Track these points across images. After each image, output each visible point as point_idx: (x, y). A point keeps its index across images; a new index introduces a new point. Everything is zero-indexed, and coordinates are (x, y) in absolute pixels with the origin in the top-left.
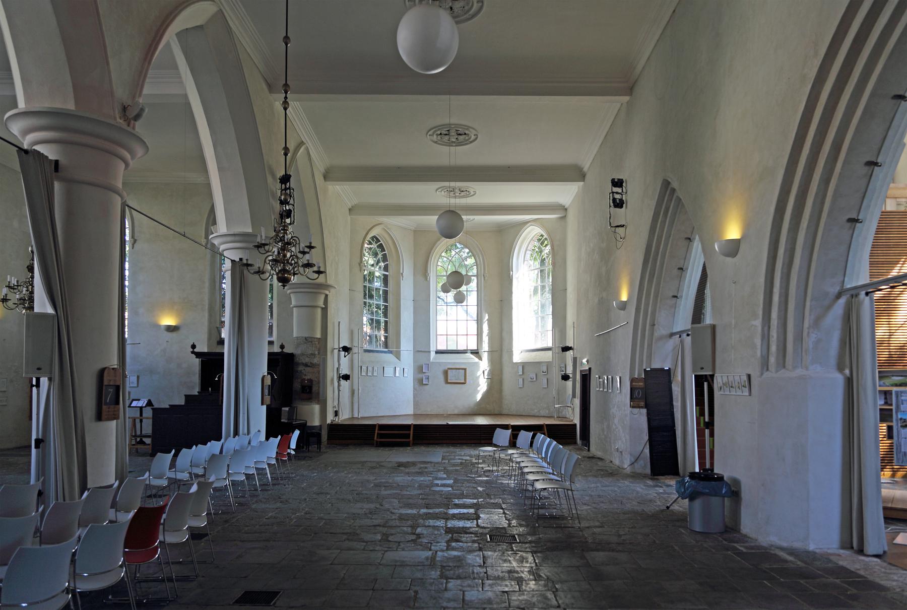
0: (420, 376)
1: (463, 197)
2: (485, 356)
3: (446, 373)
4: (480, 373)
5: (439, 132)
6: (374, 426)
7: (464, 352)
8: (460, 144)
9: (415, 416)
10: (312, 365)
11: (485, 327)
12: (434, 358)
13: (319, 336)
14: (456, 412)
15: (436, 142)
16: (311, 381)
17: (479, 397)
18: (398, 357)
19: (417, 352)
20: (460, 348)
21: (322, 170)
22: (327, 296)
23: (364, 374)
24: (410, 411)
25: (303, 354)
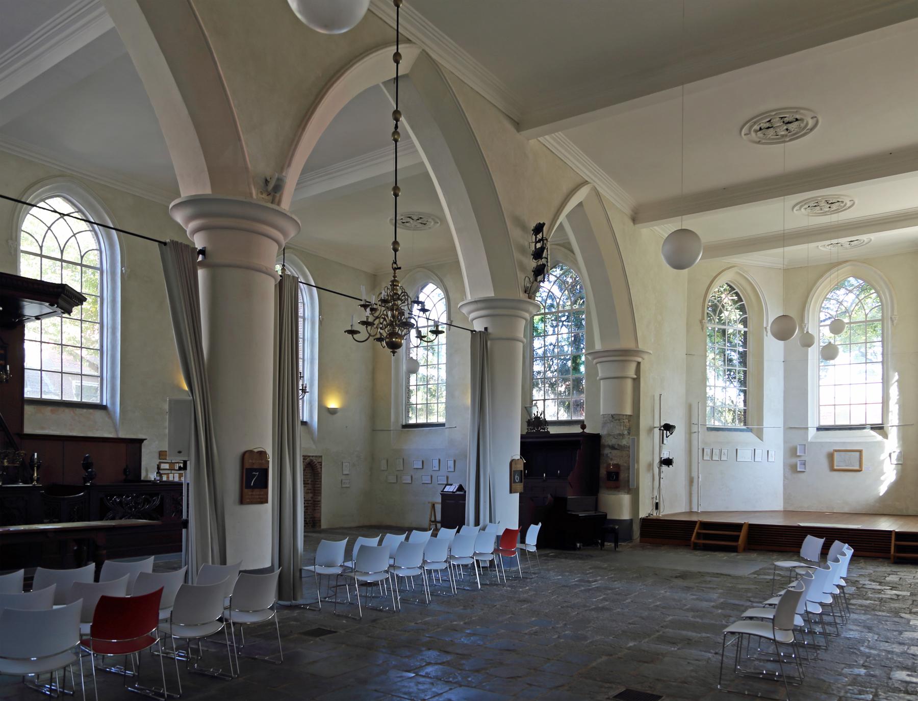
0: (794, 460)
1: (837, 211)
2: (893, 433)
3: (831, 456)
4: (884, 456)
5: (757, 127)
6: (695, 522)
7: (861, 427)
8: (795, 137)
9: (787, 513)
10: (620, 448)
11: (894, 392)
13: (628, 411)
14: (846, 510)
15: (759, 142)
16: (617, 466)
17: (883, 489)
20: (854, 422)
21: (628, 211)
22: (639, 363)
23: (707, 458)
24: (779, 505)
25: (609, 435)
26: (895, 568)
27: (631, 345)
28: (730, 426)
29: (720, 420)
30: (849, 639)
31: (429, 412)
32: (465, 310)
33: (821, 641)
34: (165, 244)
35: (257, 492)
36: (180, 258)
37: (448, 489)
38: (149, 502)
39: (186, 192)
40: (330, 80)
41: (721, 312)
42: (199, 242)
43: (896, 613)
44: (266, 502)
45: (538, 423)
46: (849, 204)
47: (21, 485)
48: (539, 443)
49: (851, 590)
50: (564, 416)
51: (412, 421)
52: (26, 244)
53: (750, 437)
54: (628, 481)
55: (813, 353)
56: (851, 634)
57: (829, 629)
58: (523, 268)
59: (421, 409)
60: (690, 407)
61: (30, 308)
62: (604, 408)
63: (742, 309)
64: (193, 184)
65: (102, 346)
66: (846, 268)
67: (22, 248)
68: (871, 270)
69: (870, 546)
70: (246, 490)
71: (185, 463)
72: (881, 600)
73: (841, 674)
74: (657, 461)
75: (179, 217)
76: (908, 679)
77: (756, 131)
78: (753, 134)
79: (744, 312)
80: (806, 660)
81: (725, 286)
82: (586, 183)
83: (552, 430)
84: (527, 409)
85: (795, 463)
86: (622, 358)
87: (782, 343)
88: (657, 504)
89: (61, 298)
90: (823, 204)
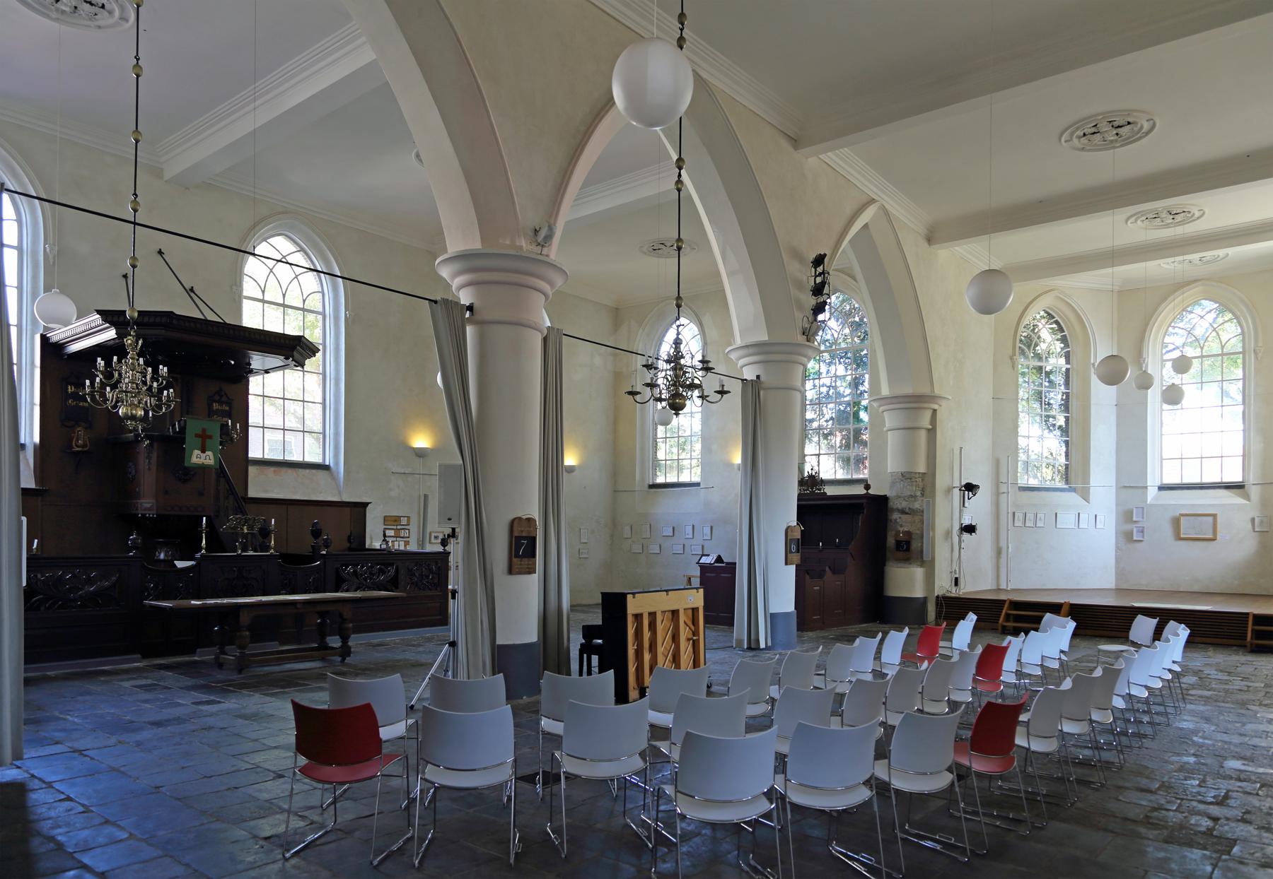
0: (1128, 527)
1: (1182, 223)
3: (1176, 522)
6: (1003, 602)
8: (1128, 141)
9: (1119, 591)
10: (912, 512)
12: (1155, 498)
14: (1196, 588)
16: (908, 533)
18: (1086, 499)
19: (1122, 488)
22: (935, 411)
24: (1109, 582)
26: (1250, 658)
27: (925, 390)
28: (1048, 484)
29: (1035, 477)
30: (1181, 729)
31: (680, 470)
32: (733, 356)
33: (1149, 730)
34: (436, 302)
35: (525, 561)
36: (451, 316)
37: (704, 560)
38: (384, 573)
39: (454, 245)
40: (599, 113)
41: (1036, 345)
42: (465, 298)
43: (1243, 704)
44: (531, 571)
45: (811, 483)
46: (1197, 214)
47: (251, 553)
48: (817, 507)
49: (1189, 680)
50: (841, 475)
51: (660, 479)
52: (249, 288)
53: (1073, 498)
54: (922, 552)
55: (1154, 395)
56: (1185, 725)
57: (1157, 719)
58: (800, 307)
59: (671, 467)
60: (997, 463)
61: (257, 360)
62: (893, 464)
63: (1064, 340)
64: (460, 237)
65: (324, 399)
66: (1197, 289)
67: (245, 293)
68: (1228, 289)
69: (1210, 630)
70: (515, 560)
71: (454, 530)
72: (1226, 691)
73: (1166, 762)
74: (956, 527)
75: (445, 272)
76: (1243, 768)
77: (1079, 137)
78: (1075, 140)
79: (1067, 345)
80: (1130, 747)
81: (1042, 313)
82: (873, 201)
83: (830, 491)
84: (801, 470)
85: (1130, 529)
86: (917, 406)
87: (1113, 389)
88: (956, 579)
89: (293, 350)
90: (1164, 215)
